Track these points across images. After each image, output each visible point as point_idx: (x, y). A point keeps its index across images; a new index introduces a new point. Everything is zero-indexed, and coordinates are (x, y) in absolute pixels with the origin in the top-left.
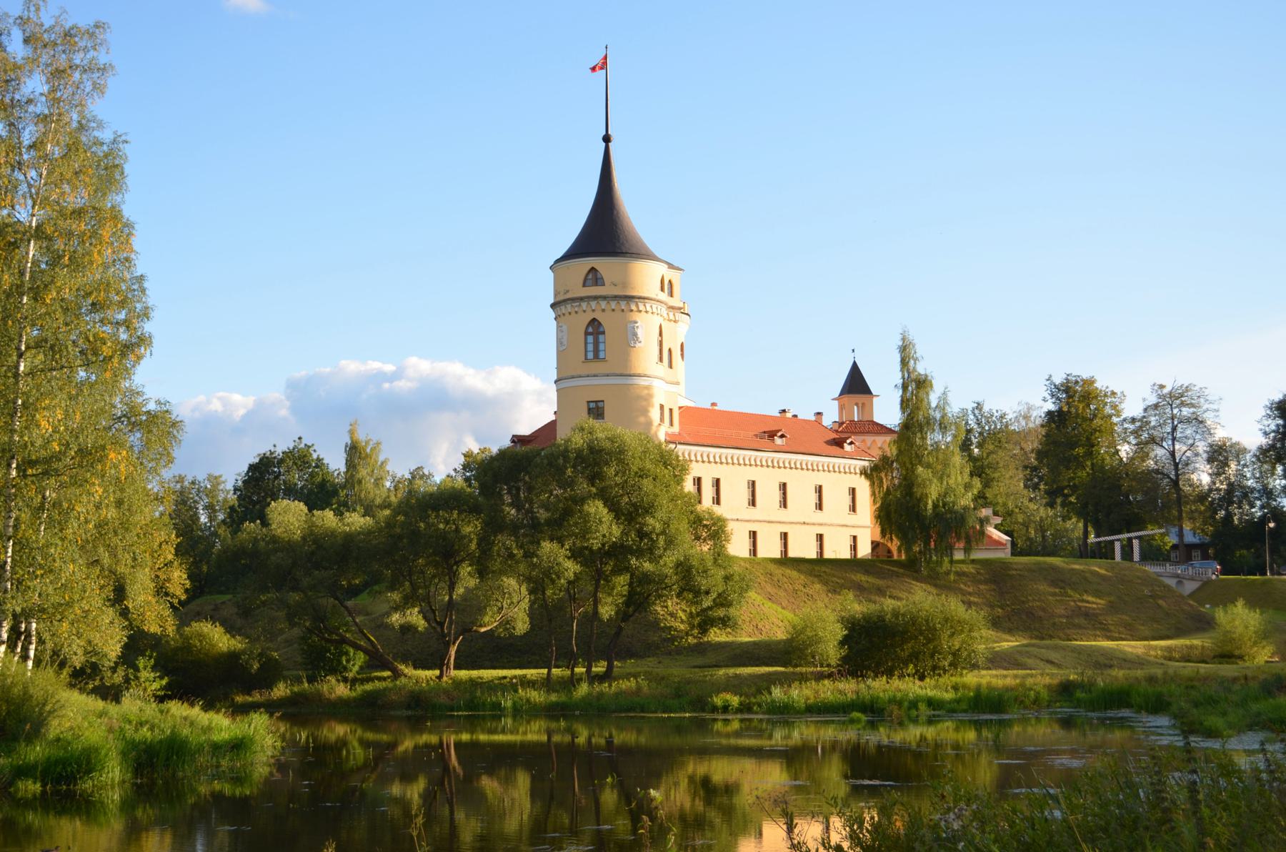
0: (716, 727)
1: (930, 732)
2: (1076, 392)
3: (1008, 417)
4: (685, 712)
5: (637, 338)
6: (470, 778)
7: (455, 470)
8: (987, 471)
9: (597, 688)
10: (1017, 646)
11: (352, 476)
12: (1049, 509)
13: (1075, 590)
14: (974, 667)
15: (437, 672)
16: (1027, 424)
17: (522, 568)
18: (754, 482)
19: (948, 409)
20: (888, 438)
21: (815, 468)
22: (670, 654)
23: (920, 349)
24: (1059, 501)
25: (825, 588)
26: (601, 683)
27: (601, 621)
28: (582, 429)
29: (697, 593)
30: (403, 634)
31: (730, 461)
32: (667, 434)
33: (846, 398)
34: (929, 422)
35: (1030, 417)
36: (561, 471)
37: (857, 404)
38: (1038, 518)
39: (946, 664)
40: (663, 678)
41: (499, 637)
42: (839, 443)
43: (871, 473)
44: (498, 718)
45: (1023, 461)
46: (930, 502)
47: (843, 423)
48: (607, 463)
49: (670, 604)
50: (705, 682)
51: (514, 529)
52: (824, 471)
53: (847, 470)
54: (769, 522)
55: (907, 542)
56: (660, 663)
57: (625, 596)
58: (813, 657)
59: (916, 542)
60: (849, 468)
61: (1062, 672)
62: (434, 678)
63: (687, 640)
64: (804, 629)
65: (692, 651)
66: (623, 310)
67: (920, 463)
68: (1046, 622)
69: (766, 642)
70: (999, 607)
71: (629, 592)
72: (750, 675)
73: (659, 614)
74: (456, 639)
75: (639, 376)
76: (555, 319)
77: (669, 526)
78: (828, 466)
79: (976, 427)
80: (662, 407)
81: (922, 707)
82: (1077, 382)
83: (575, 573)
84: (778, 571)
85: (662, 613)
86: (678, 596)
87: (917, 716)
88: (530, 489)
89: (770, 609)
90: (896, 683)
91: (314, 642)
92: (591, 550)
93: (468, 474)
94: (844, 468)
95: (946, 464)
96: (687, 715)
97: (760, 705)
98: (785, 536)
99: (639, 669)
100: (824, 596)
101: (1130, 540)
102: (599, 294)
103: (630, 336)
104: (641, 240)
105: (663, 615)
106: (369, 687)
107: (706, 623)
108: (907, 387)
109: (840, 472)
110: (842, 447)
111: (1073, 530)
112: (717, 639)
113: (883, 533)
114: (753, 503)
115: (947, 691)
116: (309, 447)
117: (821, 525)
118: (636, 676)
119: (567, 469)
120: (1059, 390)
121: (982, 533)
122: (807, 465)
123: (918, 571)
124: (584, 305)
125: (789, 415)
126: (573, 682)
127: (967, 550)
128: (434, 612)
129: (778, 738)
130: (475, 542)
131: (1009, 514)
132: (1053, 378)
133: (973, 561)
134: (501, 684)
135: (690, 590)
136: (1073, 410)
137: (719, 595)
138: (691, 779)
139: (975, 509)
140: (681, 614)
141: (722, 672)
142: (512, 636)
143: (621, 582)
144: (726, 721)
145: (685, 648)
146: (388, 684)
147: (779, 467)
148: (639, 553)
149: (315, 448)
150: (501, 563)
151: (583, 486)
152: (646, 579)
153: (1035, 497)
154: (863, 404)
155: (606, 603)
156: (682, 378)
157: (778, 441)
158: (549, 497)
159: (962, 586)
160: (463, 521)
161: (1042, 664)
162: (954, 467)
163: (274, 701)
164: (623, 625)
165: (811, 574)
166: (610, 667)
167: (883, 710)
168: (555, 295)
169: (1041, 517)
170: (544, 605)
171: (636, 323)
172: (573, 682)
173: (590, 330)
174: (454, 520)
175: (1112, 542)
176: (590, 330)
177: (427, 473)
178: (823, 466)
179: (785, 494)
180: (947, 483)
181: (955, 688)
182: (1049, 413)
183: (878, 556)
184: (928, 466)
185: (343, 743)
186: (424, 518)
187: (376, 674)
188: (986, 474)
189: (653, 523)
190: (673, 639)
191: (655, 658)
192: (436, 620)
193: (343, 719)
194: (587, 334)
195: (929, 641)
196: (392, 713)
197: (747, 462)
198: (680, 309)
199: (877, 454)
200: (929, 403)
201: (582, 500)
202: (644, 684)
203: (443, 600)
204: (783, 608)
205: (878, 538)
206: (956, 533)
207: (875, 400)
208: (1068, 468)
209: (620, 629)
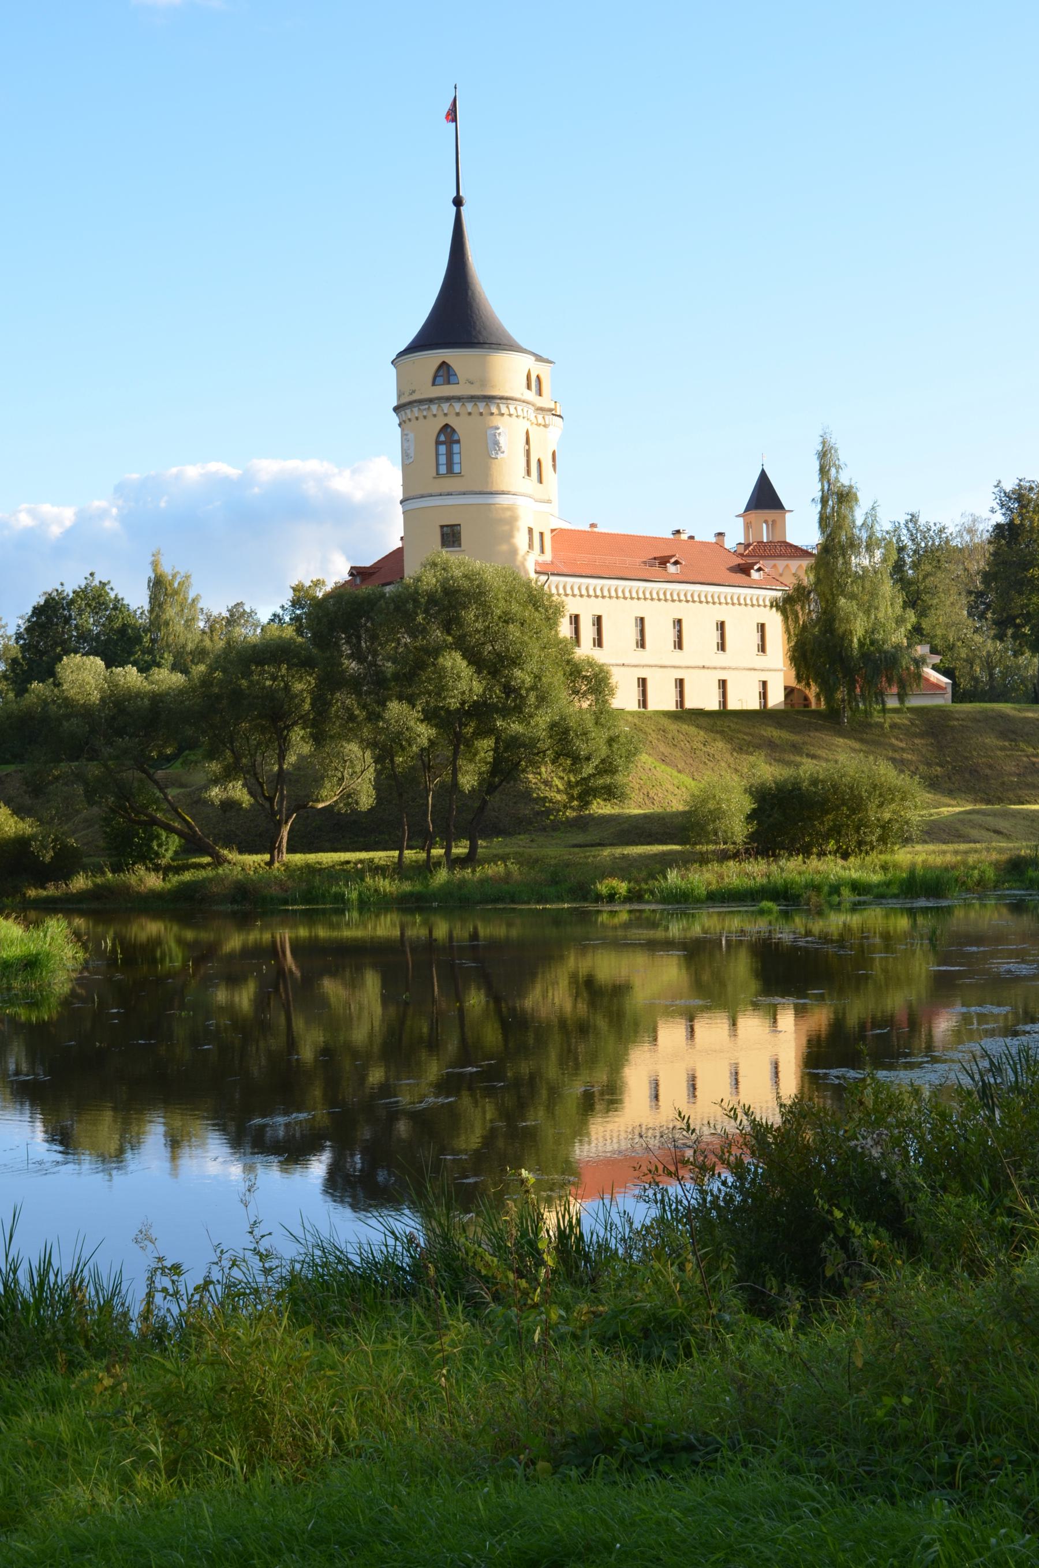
0: (600, 919)
1: (855, 920)
2: (1030, 501)
3: (948, 531)
4: (563, 901)
5: (500, 448)
6: (309, 982)
7: (283, 607)
8: (924, 597)
9: (459, 874)
10: (960, 813)
11: (158, 616)
12: (998, 643)
13: (1028, 743)
14: (907, 841)
15: (267, 857)
16: (971, 540)
17: (366, 732)
18: (642, 619)
19: (877, 527)
20: (805, 563)
21: (716, 600)
22: (544, 829)
23: (843, 455)
24: (1010, 632)
25: (729, 746)
26: (463, 868)
27: (462, 792)
28: (434, 565)
29: (576, 759)
30: (225, 812)
31: (613, 594)
32: (537, 563)
33: (754, 515)
34: (853, 544)
35: (976, 531)
36: (411, 617)
37: (766, 522)
38: (984, 653)
39: (874, 838)
40: (537, 861)
41: (339, 813)
42: (744, 570)
43: (786, 606)
44: (342, 912)
45: (966, 585)
46: (855, 640)
47: (749, 545)
48: (465, 607)
49: (543, 770)
50: (587, 864)
51: (354, 684)
52: (727, 603)
53: (755, 602)
54: (661, 667)
55: (827, 690)
56: (532, 841)
57: (490, 763)
58: (716, 834)
59: (838, 689)
60: (757, 600)
61: (1011, 845)
62: (262, 865)
63: (564, 813)
64: (704, 801)
65: (571, 826)
66: (481, 414)
67: (843, 593)
68: (993, 781)
69: (659, 814)
70: (937, 764)
71: (494, 758)
72: (640, 855)
73: (530, 782)
74: (289, 817)
75: (503, 493)
76: (400, 425)
77: (540, 679)
78: (732, 598)
79: (910, 543)
80: (530, 530)
81: (846, 892)
82: (1031, 489)
83: (429, 740)
84: (673, 727)
85: (534, 781)
86: (553, 762)
87: (839, 904)
88: (374, 638)
89: (664, 772)
90: (814, 863)
91: (119, 823)
92: (448, 711)
93: (298, 612)
94: (751, 599)
95: (874, 594)
96: (566, 906)
97: (652, 893)
98: (680, 683)
99: (507, 850)
100: (727, 755)
102: (452, 394)
103: (490, 445)
104: (504, 332)
105: (535, 784)
106: (187, 876)
107: (586, 793)
108: (827, 501)
109: (746, 605)
110: (749, 575)
111: (1026, 667)
112: (600, 811)
113: (799, 678)
114: (642, 644)
115: (874, 872)
116: (104, 584)
117: (724, 668)
118: (504, 858)
119: (417, 615)
120: (1010, 499)
121: (919, 677)
122: (706, 597)
123: (839, 723)
124: (434, 408)
125: (684, 537)
126: (429, 867)
127: (901, 697)
128: (261, 785)
129: (675, 930)
130: (308, 700)
131: (951, 648)
132: (1003, 484)
133: (911, 710)
134: (344, 870)
135: (567, 755)
136: (1027, 523)
137: (603, 761)
138: (574, 977)
139: (910, 646)
140: (557, 782)
141: (607, 852)
142: (354, 811)
143: (485, 745)
144: (613, 913)
145: (562, 823)
146: (209, 873)
147: (673, 601)
148: (506, 712)
149: (112, 585)
150: (340, 726)
151: (437, 634)
152: (514, 743)
153: (981, 627)
154: (774, 522)
155: (467, 772)
156: (554, 496)
157: (672, 569)
158: (396, 648)
159: (894, 741)
160: (293, 677)
161: (987, 835)
162: (883, 597)
163: (73, 895)
164: (488, 798)
165: (711, 729)
166: (473, 848)
167: (799, 896)
168: (399, 397)
169: (988, 652)
170: (393, 776)
171: (498, 428)
172: (429, 867)
173: (442, 438)
174: (282, 676)
176: (442, 438)
177: (248, 610)
178: (725, 598)
179: (680, 632)
180: (876, 618)
181: (884, 868)
182: (998, 527)
183: (792, 705)
184: (852, 597)
185: (156, 942)
186: (247, 674)
187: (194, 860)
188: (923, 600)
189: (521, 676)
190: (548, 812)
191: (527, 836)
192: (264, 795)
193: (156, 914)
194: (438, 443)
195: (853, 811)
196: (215, 908)
197: (634, 595)
198: (551, 410)
199: (790, 582)
200: (854, 522)
201: (436, 651)
202: (514, 868)
203: (271, 770)
204: (679, 771)
205: (793, 683)
206: (887, 676)
207: (788, 515)
208: (1021, 593)
209: (485, 802)
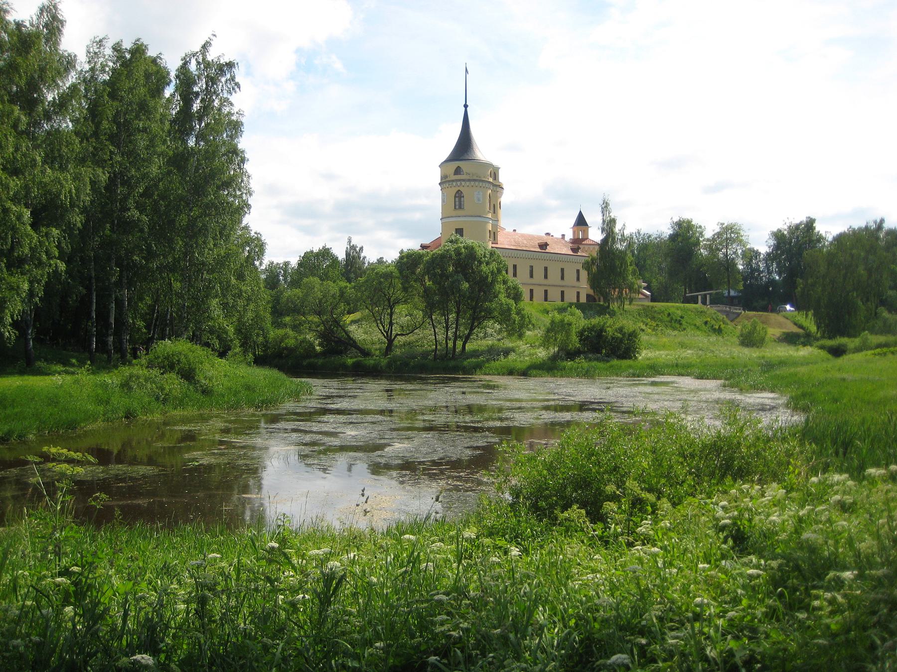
101: (705, 295)
175: (697, 296)
194: (455, 197)
